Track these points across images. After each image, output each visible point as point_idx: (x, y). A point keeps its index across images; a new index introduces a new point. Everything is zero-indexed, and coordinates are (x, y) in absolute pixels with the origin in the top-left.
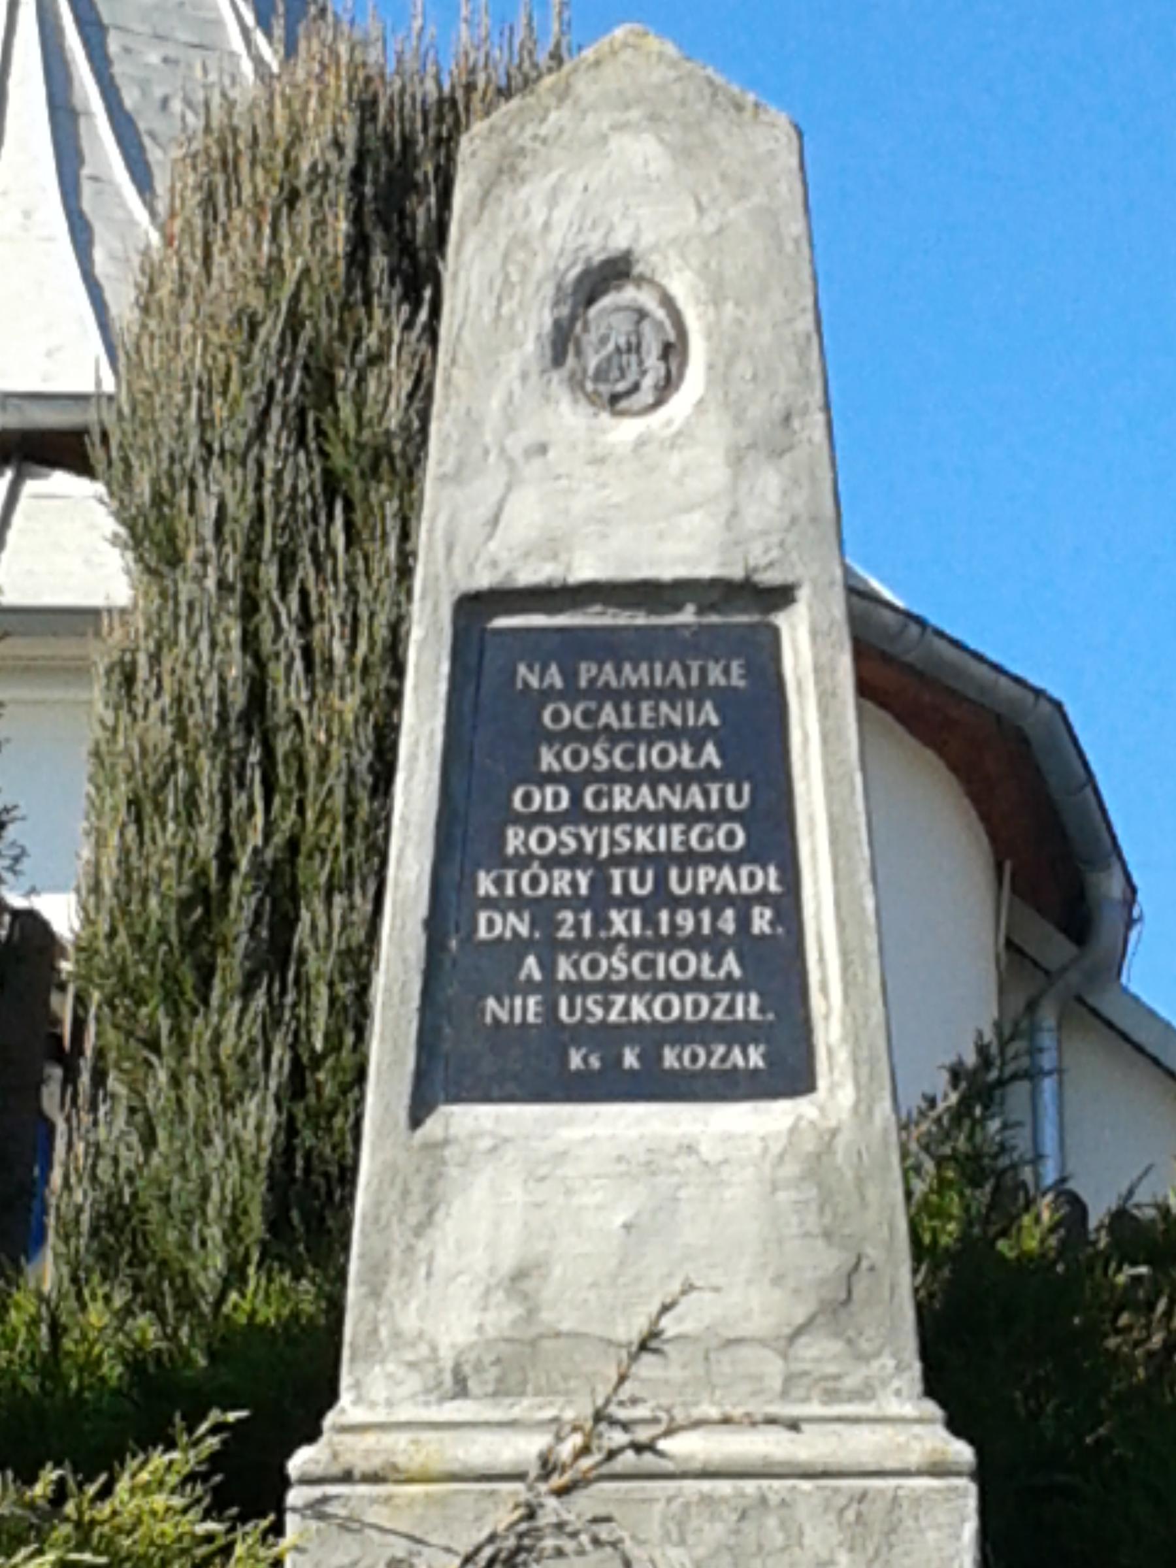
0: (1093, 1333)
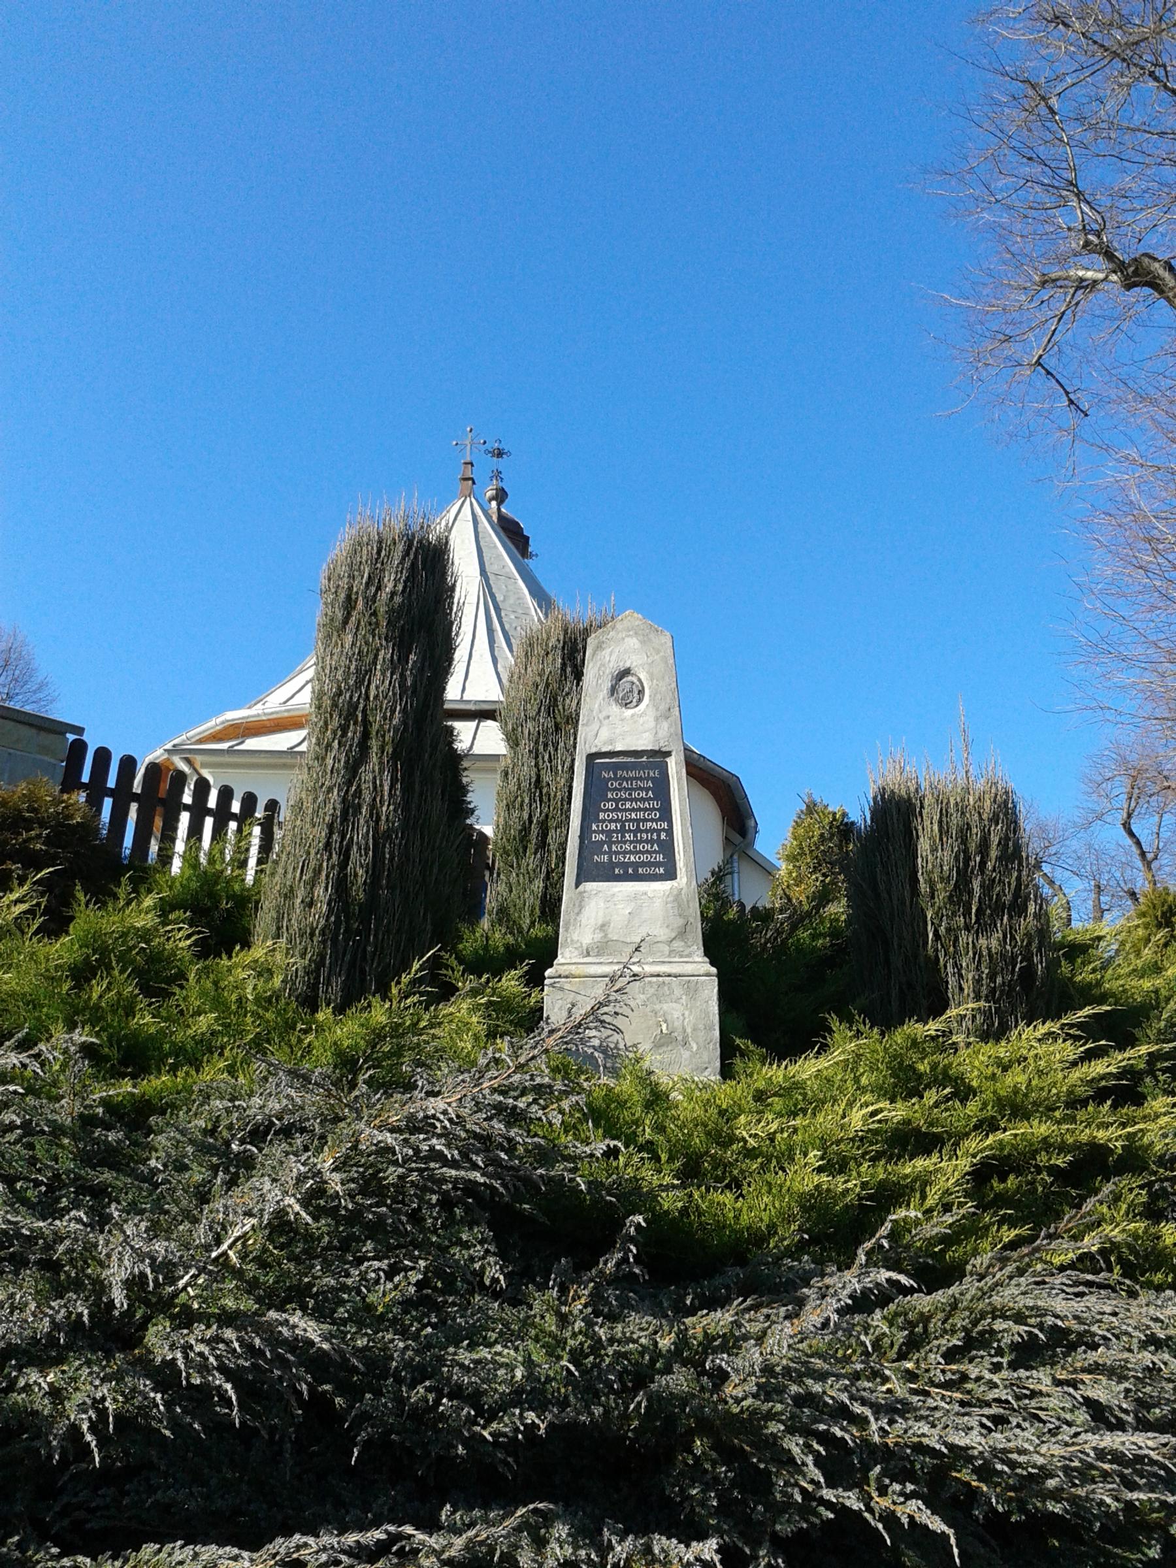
0: (747, 939)
